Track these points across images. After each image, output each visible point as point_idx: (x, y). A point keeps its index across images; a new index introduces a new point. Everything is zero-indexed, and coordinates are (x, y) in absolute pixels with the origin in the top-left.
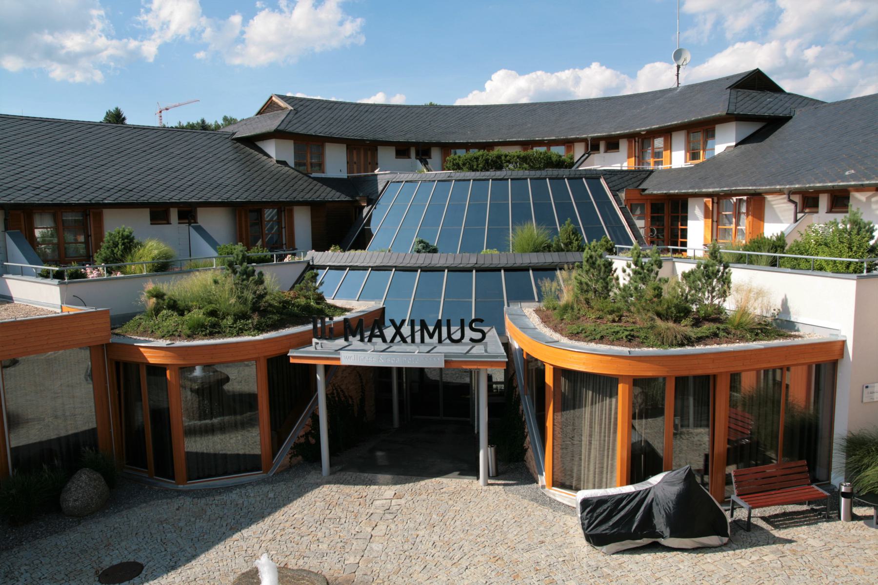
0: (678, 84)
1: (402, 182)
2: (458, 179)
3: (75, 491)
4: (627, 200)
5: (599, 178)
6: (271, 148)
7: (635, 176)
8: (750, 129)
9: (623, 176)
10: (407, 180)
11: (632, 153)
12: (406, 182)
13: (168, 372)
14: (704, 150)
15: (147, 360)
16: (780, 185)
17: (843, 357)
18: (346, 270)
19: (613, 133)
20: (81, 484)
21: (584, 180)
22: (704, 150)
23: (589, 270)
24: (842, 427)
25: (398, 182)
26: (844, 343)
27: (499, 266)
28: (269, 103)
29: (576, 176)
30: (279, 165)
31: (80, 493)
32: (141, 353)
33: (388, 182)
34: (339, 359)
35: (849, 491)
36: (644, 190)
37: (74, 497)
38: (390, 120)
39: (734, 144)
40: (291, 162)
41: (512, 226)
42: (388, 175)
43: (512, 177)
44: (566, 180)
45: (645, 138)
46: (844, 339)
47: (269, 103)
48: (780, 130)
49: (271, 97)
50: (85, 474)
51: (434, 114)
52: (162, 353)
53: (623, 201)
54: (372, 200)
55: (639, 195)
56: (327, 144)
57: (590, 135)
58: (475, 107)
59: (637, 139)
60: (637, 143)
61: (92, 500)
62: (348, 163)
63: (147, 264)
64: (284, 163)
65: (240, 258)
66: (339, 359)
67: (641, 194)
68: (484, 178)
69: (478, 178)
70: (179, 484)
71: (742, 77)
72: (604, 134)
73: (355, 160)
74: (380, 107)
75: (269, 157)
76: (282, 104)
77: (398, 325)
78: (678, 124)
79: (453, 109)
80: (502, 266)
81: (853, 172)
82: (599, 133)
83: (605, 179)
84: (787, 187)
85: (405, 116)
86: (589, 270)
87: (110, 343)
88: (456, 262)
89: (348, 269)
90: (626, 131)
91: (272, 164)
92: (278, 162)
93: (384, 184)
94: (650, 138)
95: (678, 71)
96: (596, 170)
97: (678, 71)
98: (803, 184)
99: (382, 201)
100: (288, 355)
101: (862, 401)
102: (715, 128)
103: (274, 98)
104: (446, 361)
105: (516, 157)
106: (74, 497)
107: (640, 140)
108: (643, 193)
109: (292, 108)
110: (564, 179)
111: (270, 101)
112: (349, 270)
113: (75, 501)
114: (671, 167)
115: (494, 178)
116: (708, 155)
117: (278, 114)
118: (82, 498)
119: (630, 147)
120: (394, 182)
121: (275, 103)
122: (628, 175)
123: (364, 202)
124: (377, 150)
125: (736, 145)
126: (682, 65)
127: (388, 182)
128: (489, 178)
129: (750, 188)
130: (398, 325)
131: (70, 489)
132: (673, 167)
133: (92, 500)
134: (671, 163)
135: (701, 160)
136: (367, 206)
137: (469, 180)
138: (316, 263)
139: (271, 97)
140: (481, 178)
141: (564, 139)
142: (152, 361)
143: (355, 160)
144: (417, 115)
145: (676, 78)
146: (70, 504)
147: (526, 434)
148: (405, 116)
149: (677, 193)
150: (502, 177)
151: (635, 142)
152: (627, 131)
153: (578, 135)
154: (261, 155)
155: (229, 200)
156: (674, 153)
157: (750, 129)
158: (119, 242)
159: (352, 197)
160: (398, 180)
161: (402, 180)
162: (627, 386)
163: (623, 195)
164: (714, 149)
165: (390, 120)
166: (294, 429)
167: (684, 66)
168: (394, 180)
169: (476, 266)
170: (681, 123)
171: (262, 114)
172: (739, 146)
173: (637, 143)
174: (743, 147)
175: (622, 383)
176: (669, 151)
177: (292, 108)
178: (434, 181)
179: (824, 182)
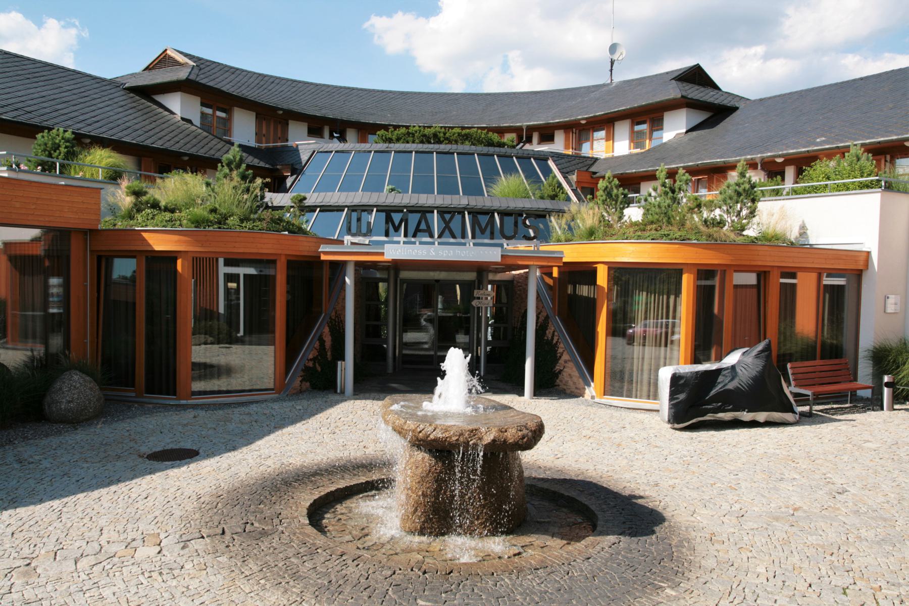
0: (612, 80)
1: (332, 152)
2: (398, 150)
3: (69, 391)
4: (578, 182)
5: (546, 160)
6: (175, 103)
7: (581, 161)
8: (699, 117)
9: (570, 160)
10: (336, 150)
11: (569, 144)
12: (336, 152)
13: (179, 262)
14: (650, 139)
15: (152, 248)
16: (751, 155)
17: (868, 269)
18: (315, 211)
19: (551, 121)
20: (74, 384)
21: (532, 159)
22: (650, 139)
23: (606, 200)
24: (868, 339)
25: (326, 152)
26: (868, 253)
27: (493, 208)
28: (162, 57)
29: (524, 155)
30: (185, 123)
31: (74, 394)
32: (144, 240)
33: (314, 152)
34: (382, 254)
35: (891, 381)
36: (595, 173)
37: (67, 398)
38: (300, 94)
39: (684, 131)
40: (197, 121)
41: (485, 183)
42: (312, 145)
43: (457, 151)
44: (514, 158)
45: (584, 129)
46: (869, 250)
47: (162, 57)
48: (727, 119)
49: (166, 50)
50: (77, 375)
51: (346, 95)
52: (175, 238)
53: (574, 184)
54: (297, 169)
55: (589, 178)
56: (236, 108)
57: (524, 124)
58: (391, 92)
59: (574, 130)
60: (574, 135)
61: (90, 403)
62: (256, 134)
63: (103, 170)
64: (189, 121)
65: (238, 159)
66: (382, 254)
67: (592, 177)
68: (427, 150)
69: (421, 150)
70: (180, 399)
71: (681, 72)
72: (541, 122)
73: (264, 132)
74: (285, 81)
75: (172, 113)
76: (181, 58)
77: (447, 220)
78: (627, 109)
79: (366, 92)
80: (495, 208)
81: (824, 139)
82: (534, 121)
83: (554, 161)
84: (759, 156)
85: (316, 93)
86: (606, 200)
87: (97, 231)
88: (445, 203)
89: (318, 209)
90: (566, 120)
91: (177, 120)
92: (183, 119)
93: (309, 154)
94: (589, 130)
95: (612, 67)
96: (543, 151)
97: (612, 67)
98: (775, 152)
99: (308, 171)
100: (320, 250)
101: (885, 311)
102: (663, 116)
103: (168, 52)
104: (502, 256)
105: (457, 135)
106: (67, 398)
107: (577, 131)
108: (594, 176)
109: (195, 64)
110: (512, 157)
111: (163, 55)
112: (320, 211)
113: (69, 402)
114: (613, 155)
115: (438, 150)
116: (655, 143)
117: (177, 69)
118: (78, 399)
119: (567, 139)
120: (321, 152)
121: (170, 57)
122: (575, 159)
123: (287, 172)
124: (288, 124)
125: (687, 132)
126: (618, 60)
127: (314, 152)
128: (432, 150)
129: (718, 160)
130: (447, 220)
131: (61, 389)
132: (615, 155)
133: (90, 403)
134: (613, 152)
135: (647, 148)
136: (291, 175)
137: (411, 152)
138: (275, 204)
139: (166, 50)
140: (424, 150)
141: (496, 127)
142: (157, 248)
143: (264, 132)
144: (329, 93)
145: (610, 74)
146: (63, 407)
147: (559, 355)
148: (316, 93)
149: (635, 172)
150: (447, 151)
151: (573, 133)
152: (568, 119)
153: (512, 123)
154: (161, 110)
155: (144, 144)
156: (615, 144)
157: (699, 117)
158: (61, 143)
159: (272, 165)
160: (326, 150)
161: (331, 150)
162: (692, 276)
163: (574, 178)
164: (662, 138)
165: (300, 94)
166: (304, 349)
167: (619, 62)
168: (320, 150)
169: (468, 207)
170: (630, 109)
171: (150, 69)
172: (689, 133)
173: (574, 135)
174: (694, 133)
175: (687, 273)
176: (611, 141)
177: (195, 64)
178: (370, 152)
179: (797, 148)
